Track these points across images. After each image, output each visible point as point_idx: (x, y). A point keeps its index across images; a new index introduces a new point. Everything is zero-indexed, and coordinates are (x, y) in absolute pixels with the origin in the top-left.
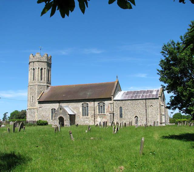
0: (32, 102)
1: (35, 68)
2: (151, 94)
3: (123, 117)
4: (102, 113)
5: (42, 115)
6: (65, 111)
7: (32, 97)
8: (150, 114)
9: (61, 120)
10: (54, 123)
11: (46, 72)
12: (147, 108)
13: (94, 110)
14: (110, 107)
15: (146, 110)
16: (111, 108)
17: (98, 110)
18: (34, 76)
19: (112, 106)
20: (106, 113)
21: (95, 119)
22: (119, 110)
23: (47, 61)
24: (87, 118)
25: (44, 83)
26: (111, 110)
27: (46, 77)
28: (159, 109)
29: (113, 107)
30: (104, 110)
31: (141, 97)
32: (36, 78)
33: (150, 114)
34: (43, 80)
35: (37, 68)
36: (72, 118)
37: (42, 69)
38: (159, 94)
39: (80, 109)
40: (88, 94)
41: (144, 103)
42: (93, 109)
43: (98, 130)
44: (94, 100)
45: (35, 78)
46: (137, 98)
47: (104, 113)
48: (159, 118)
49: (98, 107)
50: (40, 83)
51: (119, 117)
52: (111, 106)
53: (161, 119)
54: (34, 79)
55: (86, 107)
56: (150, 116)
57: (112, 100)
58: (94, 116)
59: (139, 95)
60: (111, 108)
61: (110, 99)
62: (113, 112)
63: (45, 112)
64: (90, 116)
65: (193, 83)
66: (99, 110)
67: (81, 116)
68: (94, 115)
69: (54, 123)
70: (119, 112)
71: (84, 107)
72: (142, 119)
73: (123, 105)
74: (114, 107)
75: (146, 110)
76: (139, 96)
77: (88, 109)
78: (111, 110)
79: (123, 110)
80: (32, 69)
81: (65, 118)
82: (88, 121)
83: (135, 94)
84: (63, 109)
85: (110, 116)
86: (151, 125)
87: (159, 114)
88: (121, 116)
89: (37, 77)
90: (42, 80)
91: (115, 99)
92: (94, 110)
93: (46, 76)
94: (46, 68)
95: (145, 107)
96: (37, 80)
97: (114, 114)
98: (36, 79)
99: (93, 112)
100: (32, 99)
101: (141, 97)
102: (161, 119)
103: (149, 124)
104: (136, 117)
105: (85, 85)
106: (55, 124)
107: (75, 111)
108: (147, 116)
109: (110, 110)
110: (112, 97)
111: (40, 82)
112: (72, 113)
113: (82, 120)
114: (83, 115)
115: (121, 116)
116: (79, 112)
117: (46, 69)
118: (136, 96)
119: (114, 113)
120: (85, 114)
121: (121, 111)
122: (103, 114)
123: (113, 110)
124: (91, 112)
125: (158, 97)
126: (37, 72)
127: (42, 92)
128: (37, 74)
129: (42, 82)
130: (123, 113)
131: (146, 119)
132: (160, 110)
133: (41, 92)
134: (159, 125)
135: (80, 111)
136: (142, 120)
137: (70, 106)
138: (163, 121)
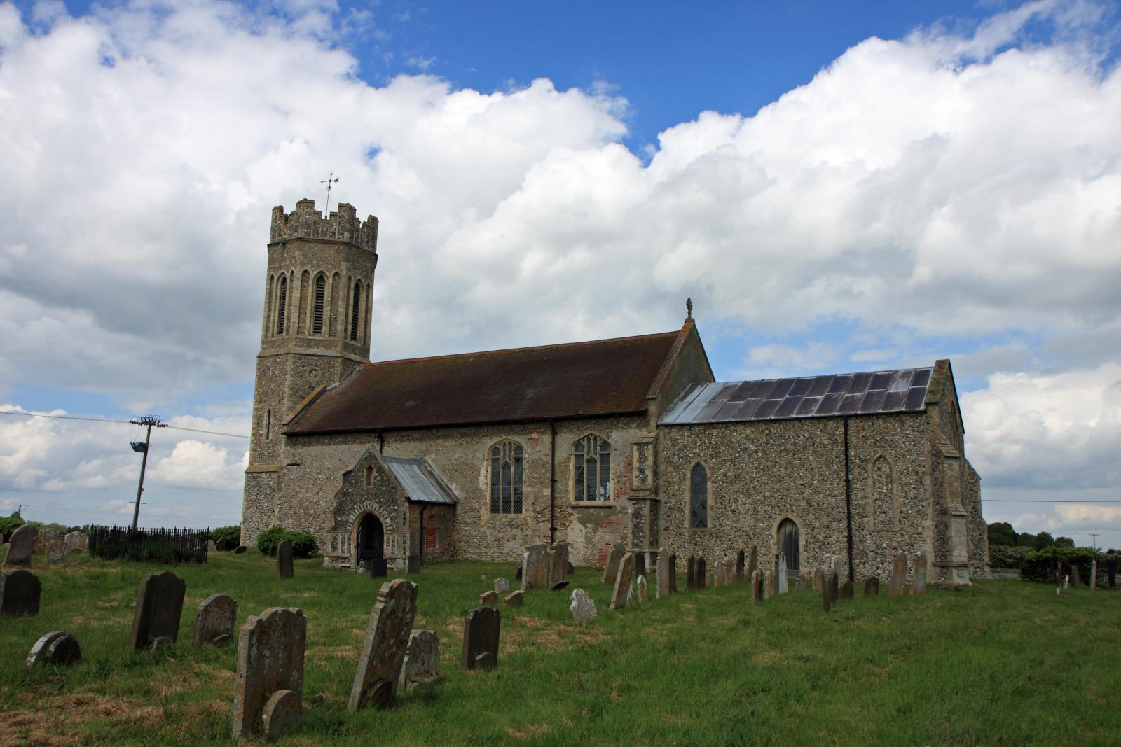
0: (264, 438)
1: (288, 275)
2: (880, 394)
3: (710, 524)
4: (592, 497)
5: (301, 503)
6: (390, 487)
7: (266, 414)
8: (870, 510)
9: (371, 529)
10: (334, 548)
11: (342, 294)
13: (553, 481)
14: (636, 464)
15: (848, 481)
16: (642, 471)
17: (571, 483)
19: (650, 460)
20: (617, 497)
21: (553, 529)
22: (688, 483)
23: (351, 238)
24: (512, 526)
25: (329, 346)
26: (643, 480)
27: (341, 318)
28: (928, 481)
29: (655, 463)
31: (815, 408)
32: (289, 319)
33: (870, 510)
34: (325, 329)
35: (298, 274)
36: (437, 518)
37: (320, 279)
38: (931, 392)
39: (483, 472)
40: (530, 393)
41: (835, 443)
42: (549, 475)
43: (918, 483)
44: (554, 424)
45: (285, 322)
46: (794, 416)
48: (929, 535)
49: (572, 465)
50: (309, 346)
51: (687, 524)
52: (642, 458)
53: (942, 541)
54: (281, 324)
55: (512, 462)
56: (870, 522)
57: (653, 424)
58: (548, 516)
59: (807, 400)
61: (639, 415)
62: (656, 492)
63: (316, 490)
64: (527, 513)
66: (579, 481)
67: (485, 513)
68: (553, 506)
69: (334, 548)
70: (687, 497)
71: (502, 462)
72: (821, 537)
73: (710, 451)
74: (662, 468)
75: (848, 481)
76: (807, 405)
77: (519, 475)
78: (643, 480)
79: (709, 485)
80: (276, 278)
81: (387, 522)
82: (519, 541)
83: (787, 396)
84: (380, 470)
85: (637, 515)
87: (930, 511)
88: (698, 520)
89: (294, 318)
90: (317, 328)
91: (669, 419)
92: (553, 481)
93: (341, 310)
94: (344, 273)
95: (838, 466)
96: (293, 328)
97: (655, 504)
98: (288, 330)
99: (547, 492)
100: (265, 423)
101: (815, 408)
102: (942, 541)
103: (863, 572)
104: (786, 521)
105: (451, 357)
106: (339, 552)
107: (453, 486)
108: (856, 520)
109: (636, 483)
110: (652, 408)
111: (309, 343)
112: (435, 496)
113: (488, 532)
114: (494, 509)
115: (698, 520)
116: (475, 493)
117: (343, 280)
118: (788, 405)
119: (662, 497)
121: (698, 490)
122: (586, 503)
123: (650, 480)
124: (534, 492)
125: (922, 407)
126: (296, 295)
127: (317, 390)
128: (296, 302)
129: (318, 344)
130: (710, 501)
131: (850, 538)
132: (938, 484)
133: (313, 388)
134: (931, 575)
136: (823, 546)
137: (433, 456)
138: (956, 552)
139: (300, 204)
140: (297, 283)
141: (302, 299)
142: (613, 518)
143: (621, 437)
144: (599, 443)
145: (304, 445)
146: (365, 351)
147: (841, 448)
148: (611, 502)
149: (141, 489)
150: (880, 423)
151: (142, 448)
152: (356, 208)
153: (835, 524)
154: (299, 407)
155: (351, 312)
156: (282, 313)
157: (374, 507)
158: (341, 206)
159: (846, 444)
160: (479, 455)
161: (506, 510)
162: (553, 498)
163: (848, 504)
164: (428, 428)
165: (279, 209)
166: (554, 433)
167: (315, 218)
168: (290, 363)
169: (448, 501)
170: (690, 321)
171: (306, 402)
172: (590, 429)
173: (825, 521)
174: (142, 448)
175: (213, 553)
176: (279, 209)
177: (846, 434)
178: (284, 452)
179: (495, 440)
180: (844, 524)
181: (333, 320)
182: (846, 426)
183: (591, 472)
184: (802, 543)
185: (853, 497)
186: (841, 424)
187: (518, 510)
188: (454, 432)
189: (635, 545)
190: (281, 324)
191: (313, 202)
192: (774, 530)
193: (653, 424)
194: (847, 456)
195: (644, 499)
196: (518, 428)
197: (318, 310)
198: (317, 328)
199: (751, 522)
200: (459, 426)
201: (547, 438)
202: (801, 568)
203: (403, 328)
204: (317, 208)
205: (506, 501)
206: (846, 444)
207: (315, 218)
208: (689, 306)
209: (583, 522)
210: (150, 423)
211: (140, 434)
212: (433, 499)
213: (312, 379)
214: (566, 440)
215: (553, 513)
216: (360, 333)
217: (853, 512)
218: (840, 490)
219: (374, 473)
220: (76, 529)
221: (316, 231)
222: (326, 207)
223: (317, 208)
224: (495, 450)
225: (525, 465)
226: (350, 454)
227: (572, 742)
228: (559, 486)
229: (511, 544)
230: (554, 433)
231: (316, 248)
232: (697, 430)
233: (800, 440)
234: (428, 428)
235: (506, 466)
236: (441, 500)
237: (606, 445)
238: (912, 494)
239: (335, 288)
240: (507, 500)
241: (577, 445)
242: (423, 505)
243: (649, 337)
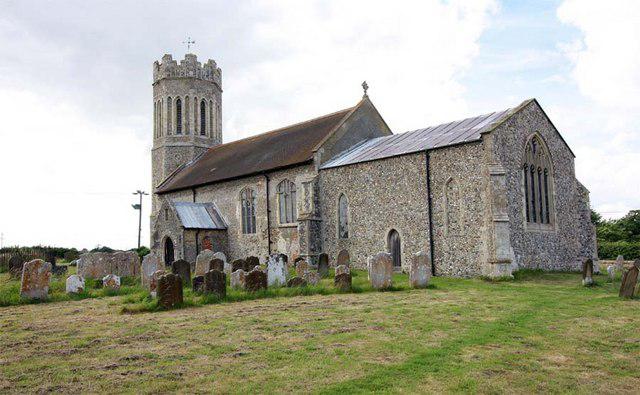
12: (434, 192)
15: (430, 199)
16: (307, 201)
17: (278, 212)
21: (270, 242)
34: (183, 130)
35: (165, 100)
41: (421, 172)
44: (267, 174)
60: (307, 201)
61: (309, 163)
64: (259, 233)
65: (604, 393)
75: (430, 199)
78: (308, 207)
86: (625, 258)
92: (269, 211)
104: (393, 232)
105: (267, 134)
111: (174, 140)
114: (244, 232)
116: (234, 221)
117: (192, 100)
120: (249, 229)
122: (290, 224)
129: (203, 141)
135: (238, 217)
141: (169, 113)
151: (138, 207)
153: (422, 233)
155: (199, 119)
159: (428, 171)
161: (249, 232)
162: (269, 223)
163: (430, 217)
166: (268, 181)
167: (172, 65)
169: (219, 227)
170: (366, 96)
174: (138, 207)
181: (187, 125)
182: (428, 157)
184: (402, 247)
185: (434, 211)
187: (254, 232)
191: (171, 56)
192: (385, 238)
193: (316, 169)
194: (429, 181)
199: (372, 233)
202: (402, 265)
203: (243, 119)
206: (428, 171)
207: (172, 65)
208: (365, 86)
209: (285, 237)
212: (206, 227)
213: (178, 161)
216: (208, 130)
217: (434, 222)
222: (179, 58)
228: (272, 214)
230: (195, 194)
232: (341, 170)
233: (399, 172)
236: (214, 226)
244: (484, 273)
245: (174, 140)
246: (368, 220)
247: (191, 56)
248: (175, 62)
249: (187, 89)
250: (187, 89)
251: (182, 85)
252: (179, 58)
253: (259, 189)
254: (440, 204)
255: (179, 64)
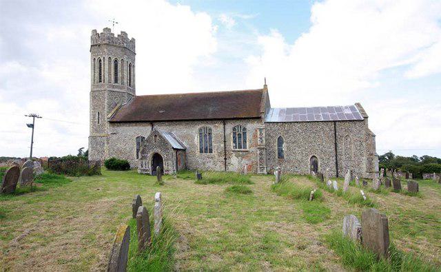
1: (102, 59)
6: (164, 143)
15: (336, 144)
16: (261, 138)
18: (100, 71)
21: (225, 159)
30: (245, 141)
39: (196, 138)
44: (224, 121)
47: (245, 147)
51: (277, 157)
52: (261, 134)
54: (100, 78)
64: (215, 153)
75: (336, 144)
82: (212, 163)
85: (261, 154)
89: (106, 76)
96: (106, 80)
99: (222, 145)
100: (97, 117)
109: (259, 143)
111: (113, 87)
112: (179, 147)
114: (201, 151)
116: (193, 145)
122: (242, 150)
124: (217, 146)
126: (107, 67)
127: (118, 105)
129: (117, 87)
139: (104, 30)
140: (107, 62)
141: (110, 68)
142: (249, 155)
143: (251, 127)
144: (242, 128)
145: (118, 126)
146: (134, 91)
147: (333, 132)
148: (248, 149)
149: (32, 142)
150: (347, 124)
151: (32, 126)
152: (127, 32)
154: (113, 111)
156: (100, 74)
157: (158, 151)
158: (122, 32)
160: (194, 131)
164: (172, 121)
165: (95, 31)
166: (224, 124)
168: (106, 94)
169: (182, 148)
170: (265, 86)
171: (115, 109)
172: (238, 123)
173: (327, 157)
174: (32, 126)
175: (103, 169)
176: (95, 31)
177: (335, 127)
178: (108, 129)
179: (200, 126)
180: (334, 158)
181: (123, 78)
182: (335, 124)
183: (240, 138)
184: (319, 165)
186: (329, 129)
187: (211, 152)
188: (183, 123)
189: (260, 165)
190: (100, 78)
195: (263, 149)
196: (209, 122)
197: (116, 74)
198: (116, 81)
199: (300, 157)
200: (176, 121)
201: (222, 126)
204: (112, 32)
205: (206, 149)
210: (34, 116)
211: (30, 121)
213: (117, 102)
214: (229, 127)
215: (226, 154)
218: (333, 146)
219: (158, 138)
220: (19, 158)
221: (112, 41)
222: (116, 32)
223: (112, 32)
224: (200, 130)
225: (213, 136)
226: (145, 131)
227: (129, 202)
229: (208, 164)
230: (224, 124)
231: (113, 48)
233: (318, 129)
234: (172, 121)
235: (205, 136)
237: (245, 129)
238: (358, 148)
239: (122, 65)
240: (206, 149)
241: (234, 129)
242: (177, 150)
243: (195, 96)
244: (364, 177)
245: (113, 87)
246: (298, 150)
247: (124, 32)
248: (113, 34)
249: (113, 53)
250: (113, 53)
251: (119, 51)
252: (100, 31)
253: (217, 129)
254: (341, 147)
255: (116, 36)
